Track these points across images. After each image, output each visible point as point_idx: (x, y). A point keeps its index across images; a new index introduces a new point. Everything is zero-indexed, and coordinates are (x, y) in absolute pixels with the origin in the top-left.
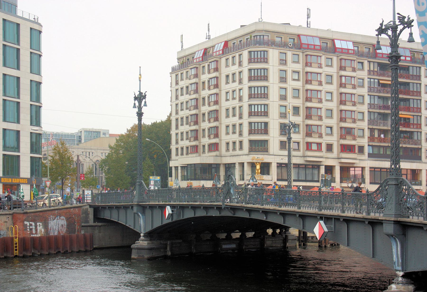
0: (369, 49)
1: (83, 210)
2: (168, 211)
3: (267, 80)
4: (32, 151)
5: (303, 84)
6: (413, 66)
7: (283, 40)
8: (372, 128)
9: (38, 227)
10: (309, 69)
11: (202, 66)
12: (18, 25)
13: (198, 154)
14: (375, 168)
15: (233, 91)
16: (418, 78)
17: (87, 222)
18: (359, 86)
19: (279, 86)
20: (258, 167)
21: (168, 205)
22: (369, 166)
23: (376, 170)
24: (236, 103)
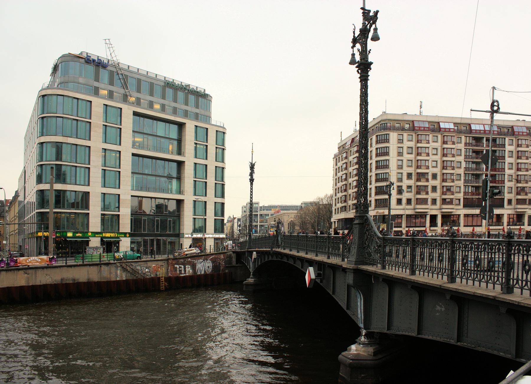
1: (227, 255)
3: (388, 155)
5: (415, 156)
6: (499, 138)
7: (459, 128)
9: (187, 269)
10: (419, 145)
11: (350, 150)
13: (346, 212)
16: (503, 147)
17: (231, 263)
18: (458, 155)
19: (397, 159)
21: (254, 251)
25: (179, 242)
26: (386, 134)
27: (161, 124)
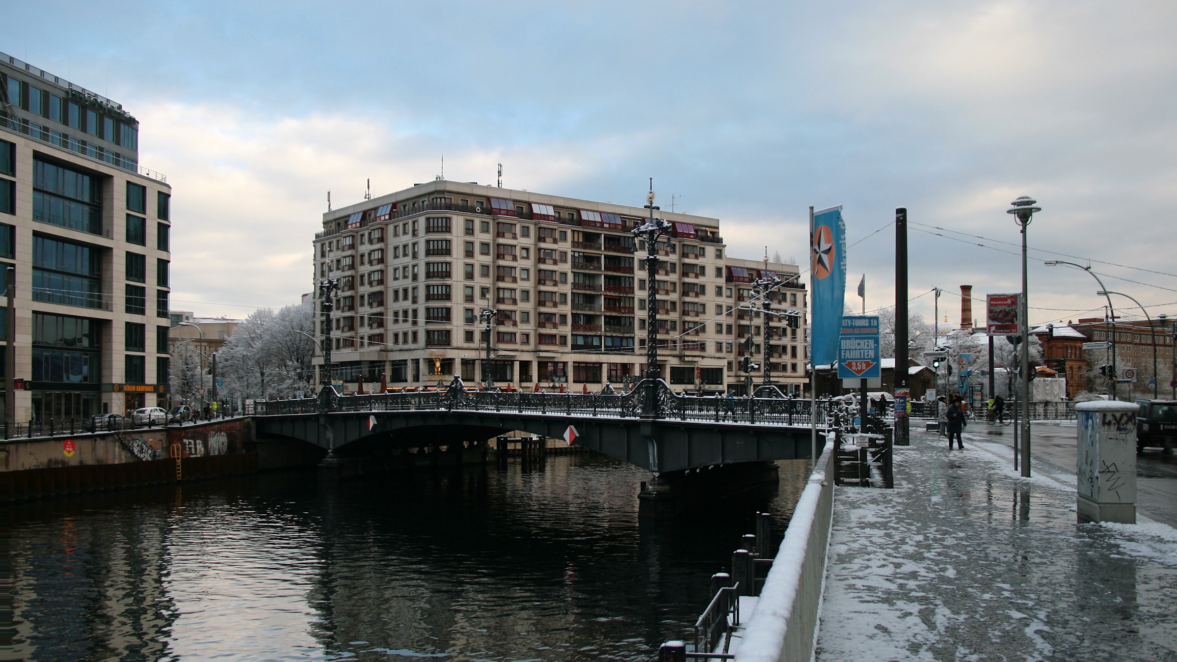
0: (573, 214)
2: (372, 422)
4: (159, 350)
5: (493, 259)
8: (577, 314)
9: (198, 446)
11: (359, 234)
12: (144, 188)
13: (353, 348)
14: (579, 363)
15: (404, 268)
20: (438, 364)
22: (572, 360)
23: (581, 365)
24: (408, 283)
25: (100, 400)
26: (446, 218)
27: (70, 175)
